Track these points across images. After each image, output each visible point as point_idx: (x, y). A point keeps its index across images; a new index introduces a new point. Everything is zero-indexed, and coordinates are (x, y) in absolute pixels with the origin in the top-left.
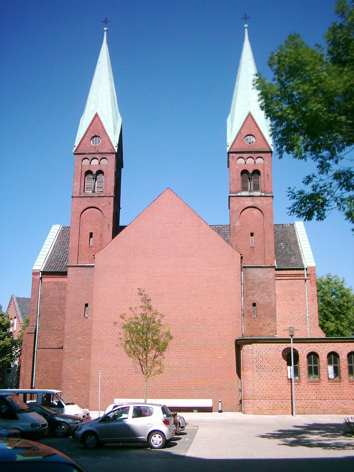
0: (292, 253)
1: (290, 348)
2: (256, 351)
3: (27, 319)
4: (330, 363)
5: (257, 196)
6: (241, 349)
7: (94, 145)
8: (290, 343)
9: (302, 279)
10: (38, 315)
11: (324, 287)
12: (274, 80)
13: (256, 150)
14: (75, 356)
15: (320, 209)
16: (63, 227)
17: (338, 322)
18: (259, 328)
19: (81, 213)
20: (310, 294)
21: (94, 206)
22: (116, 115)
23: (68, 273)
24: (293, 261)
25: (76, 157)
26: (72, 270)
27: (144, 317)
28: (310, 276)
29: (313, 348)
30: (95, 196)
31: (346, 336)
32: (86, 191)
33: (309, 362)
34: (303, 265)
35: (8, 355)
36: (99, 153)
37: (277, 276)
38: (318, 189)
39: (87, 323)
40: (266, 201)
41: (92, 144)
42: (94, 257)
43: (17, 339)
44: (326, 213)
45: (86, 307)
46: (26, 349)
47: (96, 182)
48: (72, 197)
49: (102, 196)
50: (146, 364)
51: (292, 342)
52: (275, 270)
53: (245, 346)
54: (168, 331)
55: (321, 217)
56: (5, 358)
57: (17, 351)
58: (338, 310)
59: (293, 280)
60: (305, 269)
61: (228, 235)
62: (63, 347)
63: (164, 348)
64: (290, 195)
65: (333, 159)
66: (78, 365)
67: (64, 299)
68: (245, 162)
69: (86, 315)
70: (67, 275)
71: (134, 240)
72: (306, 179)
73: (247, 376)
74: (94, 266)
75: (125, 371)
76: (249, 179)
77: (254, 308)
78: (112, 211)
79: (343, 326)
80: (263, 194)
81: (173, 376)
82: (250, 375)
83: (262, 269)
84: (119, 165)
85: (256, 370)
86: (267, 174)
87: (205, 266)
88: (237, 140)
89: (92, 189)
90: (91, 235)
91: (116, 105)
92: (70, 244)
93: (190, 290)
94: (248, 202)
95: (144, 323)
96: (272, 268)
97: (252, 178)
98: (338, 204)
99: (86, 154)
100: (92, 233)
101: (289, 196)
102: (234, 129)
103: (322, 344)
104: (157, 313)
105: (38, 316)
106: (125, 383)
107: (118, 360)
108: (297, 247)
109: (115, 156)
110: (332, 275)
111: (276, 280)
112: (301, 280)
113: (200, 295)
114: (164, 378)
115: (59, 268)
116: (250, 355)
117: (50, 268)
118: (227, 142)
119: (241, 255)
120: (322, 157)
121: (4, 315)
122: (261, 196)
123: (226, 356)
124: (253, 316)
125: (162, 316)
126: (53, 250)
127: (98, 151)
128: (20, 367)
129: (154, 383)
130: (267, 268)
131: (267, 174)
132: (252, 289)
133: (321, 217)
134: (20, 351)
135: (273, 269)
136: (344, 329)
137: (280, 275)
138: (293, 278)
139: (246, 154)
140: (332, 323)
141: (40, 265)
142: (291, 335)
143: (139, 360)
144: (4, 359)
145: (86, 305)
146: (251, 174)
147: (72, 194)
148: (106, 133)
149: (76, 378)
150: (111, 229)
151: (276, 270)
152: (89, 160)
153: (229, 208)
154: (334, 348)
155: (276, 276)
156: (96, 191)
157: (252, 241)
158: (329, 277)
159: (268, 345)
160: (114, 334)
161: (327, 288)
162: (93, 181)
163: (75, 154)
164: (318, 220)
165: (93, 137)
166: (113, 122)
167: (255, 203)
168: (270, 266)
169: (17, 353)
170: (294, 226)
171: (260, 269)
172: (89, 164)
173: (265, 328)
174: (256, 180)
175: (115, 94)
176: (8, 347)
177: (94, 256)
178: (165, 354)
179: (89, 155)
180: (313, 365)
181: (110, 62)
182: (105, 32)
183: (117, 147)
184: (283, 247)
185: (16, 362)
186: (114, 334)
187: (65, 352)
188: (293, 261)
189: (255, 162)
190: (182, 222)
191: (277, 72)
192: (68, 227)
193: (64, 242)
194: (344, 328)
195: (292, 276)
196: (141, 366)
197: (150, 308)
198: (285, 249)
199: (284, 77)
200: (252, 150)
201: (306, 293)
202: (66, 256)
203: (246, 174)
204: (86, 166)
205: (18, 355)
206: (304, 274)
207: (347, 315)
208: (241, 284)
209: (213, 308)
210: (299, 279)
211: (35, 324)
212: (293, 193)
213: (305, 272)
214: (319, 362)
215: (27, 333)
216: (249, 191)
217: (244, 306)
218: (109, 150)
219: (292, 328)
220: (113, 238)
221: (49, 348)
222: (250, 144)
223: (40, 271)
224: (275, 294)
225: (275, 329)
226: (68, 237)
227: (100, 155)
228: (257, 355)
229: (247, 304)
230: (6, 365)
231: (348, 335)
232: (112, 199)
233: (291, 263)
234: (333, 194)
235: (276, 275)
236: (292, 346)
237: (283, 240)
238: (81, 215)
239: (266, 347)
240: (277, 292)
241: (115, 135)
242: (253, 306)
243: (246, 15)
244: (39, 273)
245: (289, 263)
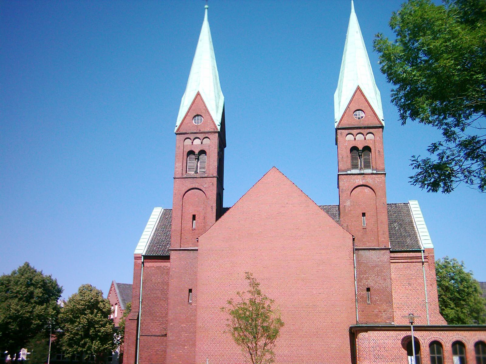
0: (407, 234)
1: (410, 337)
3: (128, 306)
4: (455, 353)
6: (356, 337)
7: (196, 124)
8: (410, 330)
10: (141, 301)
11: (441, 271)
12: (396, 42)
13: (367, 126)
15: (447, 180)
16: (165, 210)
17: (458, 309)
18: (374, 315)
19: (183, 195)
22: (218, 94)
23: (171, 257)
24: (408, 242)
25: (178, 137)
26: (175, 254)
27: (253, 302)
28: (427, 259)
29: (436, 336)
30: (197, 177)
31: (468, 324)
32: (189, 172)
33: (432, 351)
34: (419, 247)
35: (109, 342)
36: (202, 133)
37: (392, 258)
38: (445, 159)
39: (191, 309)
40: (378, 178)
41: (194, 123)
42: (197, 240)
43: (118, 326)
44: (454, 185)
45: (190, 293)
46: (128, 336)
47: (198, 163)
48: (174, 178)
49: (205, 176)
50: (256, 353)
51: (412, 330)
52: (389, 252)
53: (361, 334)
54: (278, 317)
55: (448, 189)
56: (106, 345)
57: (119, 339)
58: (458, 296)
59: (409, 263)
60: (422, 251)
61: (337, 216)
62: (166, 334)
63: (275, 336)
64: (414, 164)
65: (458, 126)
66: (182, 353)
67: (167, 284)
68: (355, 138)
69: (190, 301)
70: (170, 260)
71: (239, 222)
72: (431, 147)
74: (198, 249)
75: (232, 360)
76: (359, 156)
77: (368, 293)
78: (215, 192)
79: (464, 313)
80: (375, 172)
84: (222, 144)
87: (314, 249)
88: (345, 116)
89: (195, 170)
90: (194, 217)
91: (218, 83)
92: (173, 227)
93: (299, 274)
94: (359, 180)
95: (253, 309)
96: (386, 251)
97: (363, 155)
98: (465, 176)
100: (195, 215)
101: (412, 165)
102: (341, 104)
103: (446, 332)
104: (266, 298)
105: (141, 302)
108: (412, 228)
109: (217, 136)
110: (450, 258)
111: (391, 263)
113: (309, 279)
115: (161, 252)
116: (367, 343)
117: (152, 252)
118: (335, 118)
119: (353, 236)
120: (446, 124)
121: (104, 301)
122: (372, 174)
123: (340, 344)
124: (367, 301)
125: (272, 301)
126: (154, 233)
127: (200, 131)
128: (122, 355)
130: (381, 251)
132: (365, 273)
133: (448, 189)
134: (121, 338)
135: (388, 251)
136: (466, 316)
137: (394, 258)
138: (409, 260)
139: (355, 130)
140: (451, 310)
141: (142, 249)
142: (411, 322)
143: (249, 348)
144: (106, 347)
145: (190, 291)
146: (362, 151)
147: (174, 176)
148: (208, 112)
150: (215, 211)
151: (391, 252)
152: (191, 139)
153: (338, 187)
154: (459, 336)
155: (391, 259)
156: (198, 171)
157: (364, 222)
158: (446, 260)
159: (381, 332)
160: (220, 321)
161: (445, 272)
162: (195, 161)
163: (177, 134)
164: (444, 193)
165: (195, 116)
166: (216, 101)
167: (366, 181)
169: (118, 340)
170: (408, 206)
171: (374, 251)
172: (191, 143)
173: (381, 315)
174: (366, 157)
175: (217, 72)
176: (109, 335)
177: (198, 239)
178: (276, 341)
179: (191, 135)
180: (436, 355)
181: (211, 40)
183: (219, 126)
184: (397, 228)
185: (118, 350)
187: (168, 339)
188: (408, 242)
189: (365, 138)
191: (400, 33)
192: (169, 210)
193: (166, 225)
194: (465, 315)
195: (408, 259)
196: (251, 355)
197: (259, 293)
198: (399, 230)
199: (407, 38)
201: (425, 277)
202: (168, 239)
203: (355, 151)
205: (119, 342)
206: (422, 257)
207: (468, 302)
208: (354, 267)
210: (415, 262)
211: (137, 310)
212: (417, 162)
213: (422, 255)
214: (443, 353)
215: (130, 320)
216: (359, 169)
217: (357, 291)
219: (412, 314)
220: (217, 220)
221: (152, 335)
222: (359, 120)
223: (142, 255)
224: (391, 279)
225: (392, 315)
226: (170, 220)
227: (202, 134)
229: (360, 289)
230: (108, 353)
231: (470, 323)
232: (215, 179)
233: (406, 244)
234: (462, 163)
235: (391, 258)
236: (413, 334)
237: (397, 220)
238: (184, 196)
239: (383, 335)
240: (393, 276)
241: (218, 113)
242: (367, 291)
244: (141, 257)
245: (405, 245)
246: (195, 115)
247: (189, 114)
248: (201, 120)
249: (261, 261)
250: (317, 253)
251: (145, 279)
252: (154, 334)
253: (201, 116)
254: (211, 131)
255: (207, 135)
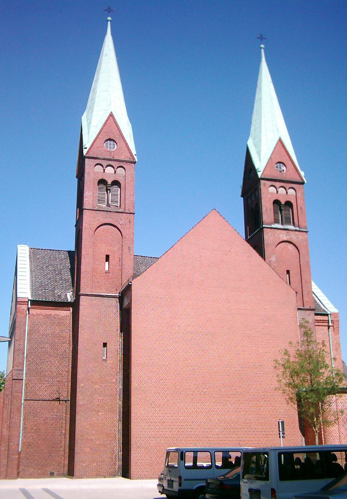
2: (340, 402)
5: (292, 230)
9: (325, 326)
10: (25, 356)
14: (92, 410)
16: (31, 249)
20: (334, 343)
21: (110, 223)
36: (116, 160)
40: (301, 236)
66: (96, 421)
73: (332, 431)
80: (298, 229)
81: (231, 433)
82: (336, 430)
83: (301, 311)
85: (342, 424)
86: (301, 207)
94: (283, 235)
96: (311, 311)
99: (100, 159)
100: (109, 255)
106: (175, 442)
107: (166, 414)
111: (316, 326)
112: (324, 327)
114: (220, 436)
122: (296, 230)
129: (209, 442)
130: (306, 311)
131: (301, 207)
149: (93, 437)
151: (316, 314)
155: (316, 322)
165: (107, 140)
168: (309, 308)
179: (103, 161)
182: (109, 23)
186: (160, 381)
190: (231, 250)
192: (37, 249)
200: (284, 179)
204: (99, 173)
209: (271, 353)
210: (322, 326)
218: (127, 158)
222: (280, 173)
227: (116, 162)
228: (341, 407)
243: (261, 35)
244: (28, 302)
246: (107, 139)
247: (100, 136)
248: (114, 145)
249: (204, 313)
250: (262, 308)
251: (31, 329)
252: (41, 398)
253: (114, 141)
254: (126, 160)
255: (121, 164)
